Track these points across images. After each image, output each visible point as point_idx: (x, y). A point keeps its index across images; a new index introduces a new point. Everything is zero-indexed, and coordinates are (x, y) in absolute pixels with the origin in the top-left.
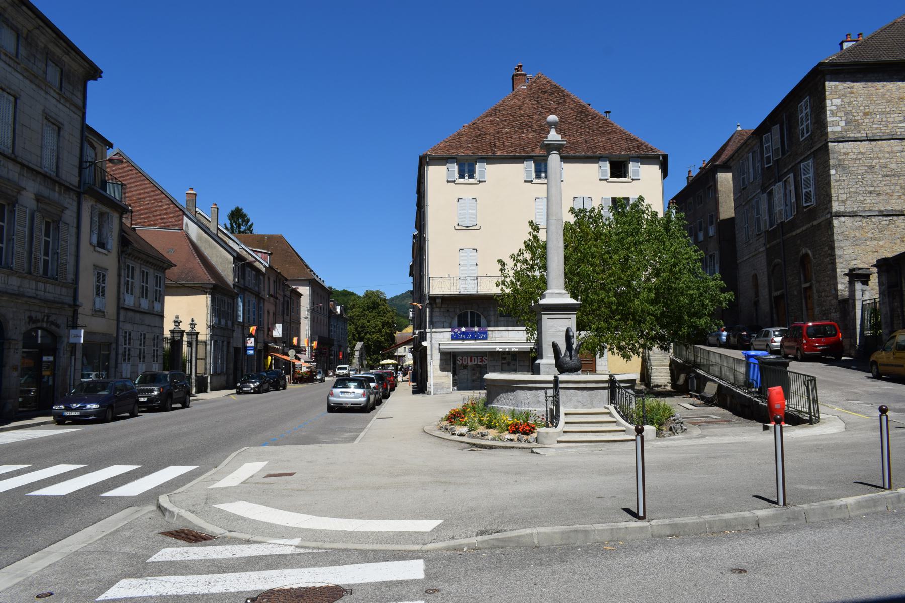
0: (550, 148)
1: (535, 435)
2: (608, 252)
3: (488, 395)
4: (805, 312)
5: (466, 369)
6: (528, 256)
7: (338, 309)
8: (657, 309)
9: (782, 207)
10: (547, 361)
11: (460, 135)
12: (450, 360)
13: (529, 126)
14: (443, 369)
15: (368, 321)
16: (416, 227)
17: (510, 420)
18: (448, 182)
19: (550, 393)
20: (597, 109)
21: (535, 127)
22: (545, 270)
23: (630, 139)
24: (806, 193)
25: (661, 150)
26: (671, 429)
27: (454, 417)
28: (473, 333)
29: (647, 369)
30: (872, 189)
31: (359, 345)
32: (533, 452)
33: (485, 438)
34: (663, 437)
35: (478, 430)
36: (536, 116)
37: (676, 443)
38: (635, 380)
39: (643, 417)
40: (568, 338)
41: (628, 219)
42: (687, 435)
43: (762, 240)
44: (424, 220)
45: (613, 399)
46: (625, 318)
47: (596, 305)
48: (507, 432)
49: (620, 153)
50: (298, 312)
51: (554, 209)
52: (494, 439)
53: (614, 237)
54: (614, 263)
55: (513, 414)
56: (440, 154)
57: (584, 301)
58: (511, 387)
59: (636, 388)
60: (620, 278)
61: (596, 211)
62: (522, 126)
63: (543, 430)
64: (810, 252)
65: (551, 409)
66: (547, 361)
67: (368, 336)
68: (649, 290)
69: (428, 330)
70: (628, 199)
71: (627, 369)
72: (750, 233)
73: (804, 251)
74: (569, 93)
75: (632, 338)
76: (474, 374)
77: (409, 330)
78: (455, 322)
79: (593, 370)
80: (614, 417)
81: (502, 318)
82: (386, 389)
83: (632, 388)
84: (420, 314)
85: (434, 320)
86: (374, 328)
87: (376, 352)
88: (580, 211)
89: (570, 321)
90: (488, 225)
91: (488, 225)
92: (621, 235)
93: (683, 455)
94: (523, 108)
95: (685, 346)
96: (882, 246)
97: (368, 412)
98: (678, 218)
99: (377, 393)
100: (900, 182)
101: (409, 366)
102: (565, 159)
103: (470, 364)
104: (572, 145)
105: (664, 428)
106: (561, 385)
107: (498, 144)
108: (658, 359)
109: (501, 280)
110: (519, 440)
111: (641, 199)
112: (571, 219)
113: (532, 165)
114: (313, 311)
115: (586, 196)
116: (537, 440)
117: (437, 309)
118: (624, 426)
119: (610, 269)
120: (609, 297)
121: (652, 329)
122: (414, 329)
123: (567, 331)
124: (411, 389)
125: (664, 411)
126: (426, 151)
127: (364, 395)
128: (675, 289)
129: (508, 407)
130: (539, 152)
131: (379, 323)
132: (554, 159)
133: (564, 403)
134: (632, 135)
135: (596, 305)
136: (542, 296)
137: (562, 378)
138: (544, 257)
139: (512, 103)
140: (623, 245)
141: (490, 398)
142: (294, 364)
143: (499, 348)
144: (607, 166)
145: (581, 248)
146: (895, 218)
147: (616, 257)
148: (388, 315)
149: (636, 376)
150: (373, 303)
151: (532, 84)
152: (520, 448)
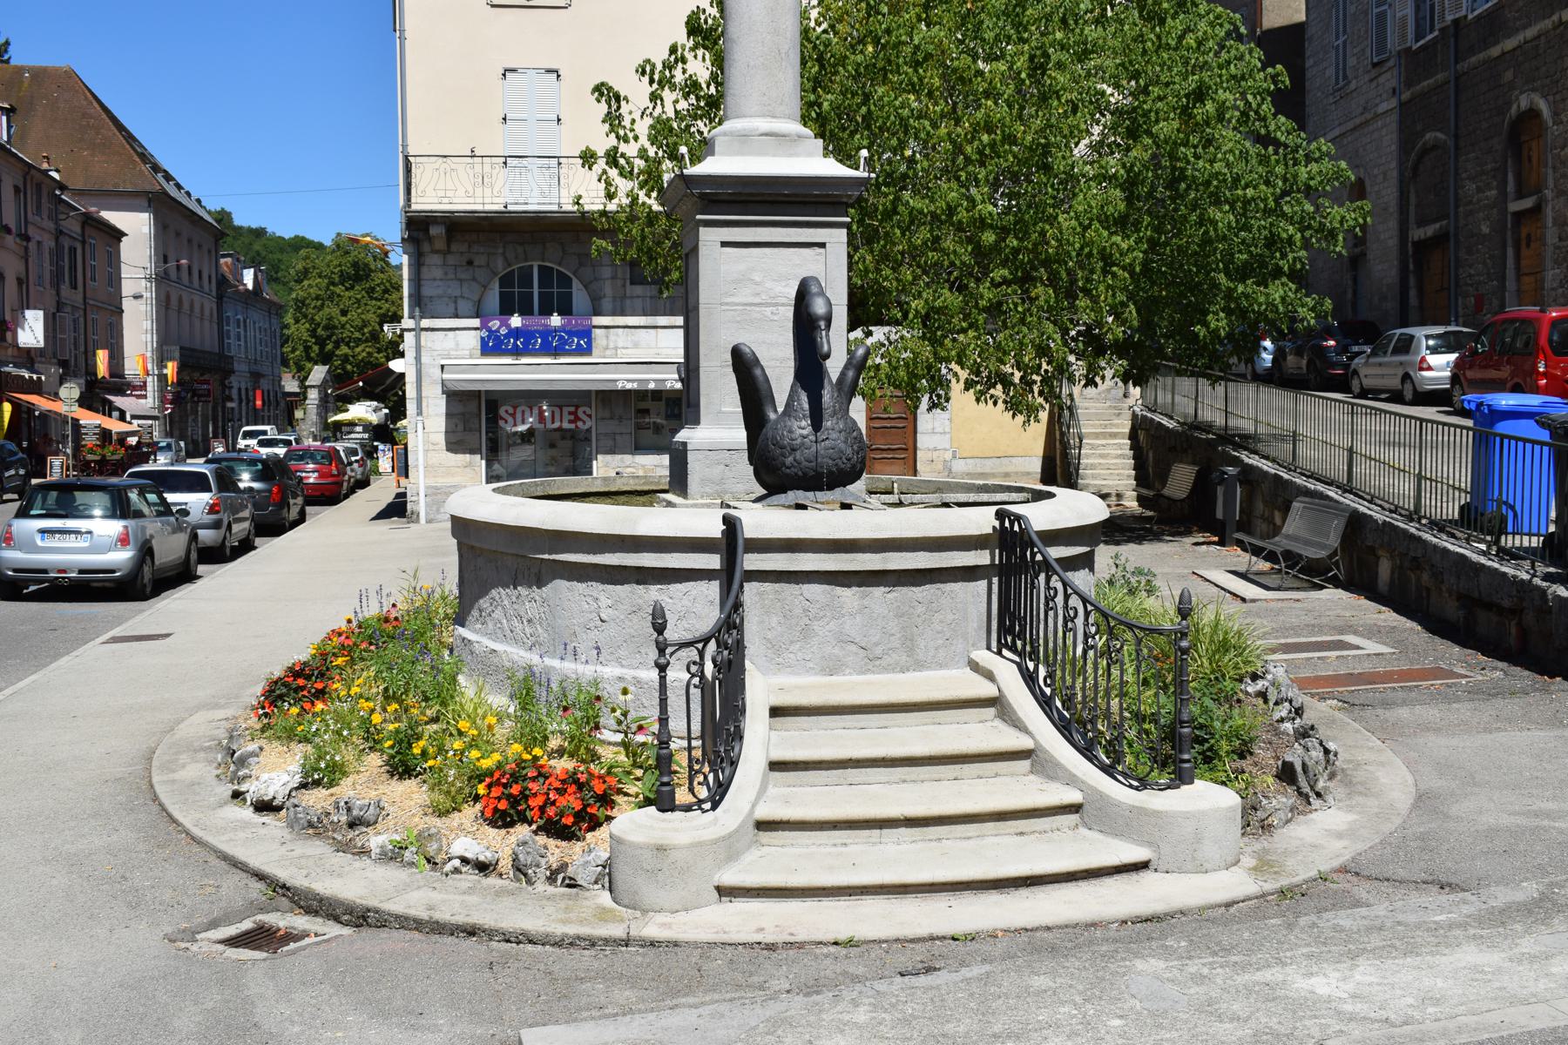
4: (1511, 284)
7: (248, 277)
10: (718, 431)
14: (454, 445)
15: (344, 313)
28: (548, 333)
29: (1065, 446)
31: (318, 373)
40: (807, 327)
43: (1389, 79)
45: (1011, 627)
50: (115, 280)
64: (1543, 106)
66: (718, 431)
67: (344, 350)
72: (1351, 61)
73: (1524, 102)
78: (493, 299)
81: (638, 290)
85: (427, 291)
86: (360, 329)
89: (826, 259)
106: (752, 562)
108: (1098, 416)
114: (162, 278)
116: (608, 876)
117: (435, 259)
118: (1072, 780)
127: (124, 541)
131: (372, 317)
133: (775, 648)
142: (75, 421)
143: (626, 380)
150: (355, 265)
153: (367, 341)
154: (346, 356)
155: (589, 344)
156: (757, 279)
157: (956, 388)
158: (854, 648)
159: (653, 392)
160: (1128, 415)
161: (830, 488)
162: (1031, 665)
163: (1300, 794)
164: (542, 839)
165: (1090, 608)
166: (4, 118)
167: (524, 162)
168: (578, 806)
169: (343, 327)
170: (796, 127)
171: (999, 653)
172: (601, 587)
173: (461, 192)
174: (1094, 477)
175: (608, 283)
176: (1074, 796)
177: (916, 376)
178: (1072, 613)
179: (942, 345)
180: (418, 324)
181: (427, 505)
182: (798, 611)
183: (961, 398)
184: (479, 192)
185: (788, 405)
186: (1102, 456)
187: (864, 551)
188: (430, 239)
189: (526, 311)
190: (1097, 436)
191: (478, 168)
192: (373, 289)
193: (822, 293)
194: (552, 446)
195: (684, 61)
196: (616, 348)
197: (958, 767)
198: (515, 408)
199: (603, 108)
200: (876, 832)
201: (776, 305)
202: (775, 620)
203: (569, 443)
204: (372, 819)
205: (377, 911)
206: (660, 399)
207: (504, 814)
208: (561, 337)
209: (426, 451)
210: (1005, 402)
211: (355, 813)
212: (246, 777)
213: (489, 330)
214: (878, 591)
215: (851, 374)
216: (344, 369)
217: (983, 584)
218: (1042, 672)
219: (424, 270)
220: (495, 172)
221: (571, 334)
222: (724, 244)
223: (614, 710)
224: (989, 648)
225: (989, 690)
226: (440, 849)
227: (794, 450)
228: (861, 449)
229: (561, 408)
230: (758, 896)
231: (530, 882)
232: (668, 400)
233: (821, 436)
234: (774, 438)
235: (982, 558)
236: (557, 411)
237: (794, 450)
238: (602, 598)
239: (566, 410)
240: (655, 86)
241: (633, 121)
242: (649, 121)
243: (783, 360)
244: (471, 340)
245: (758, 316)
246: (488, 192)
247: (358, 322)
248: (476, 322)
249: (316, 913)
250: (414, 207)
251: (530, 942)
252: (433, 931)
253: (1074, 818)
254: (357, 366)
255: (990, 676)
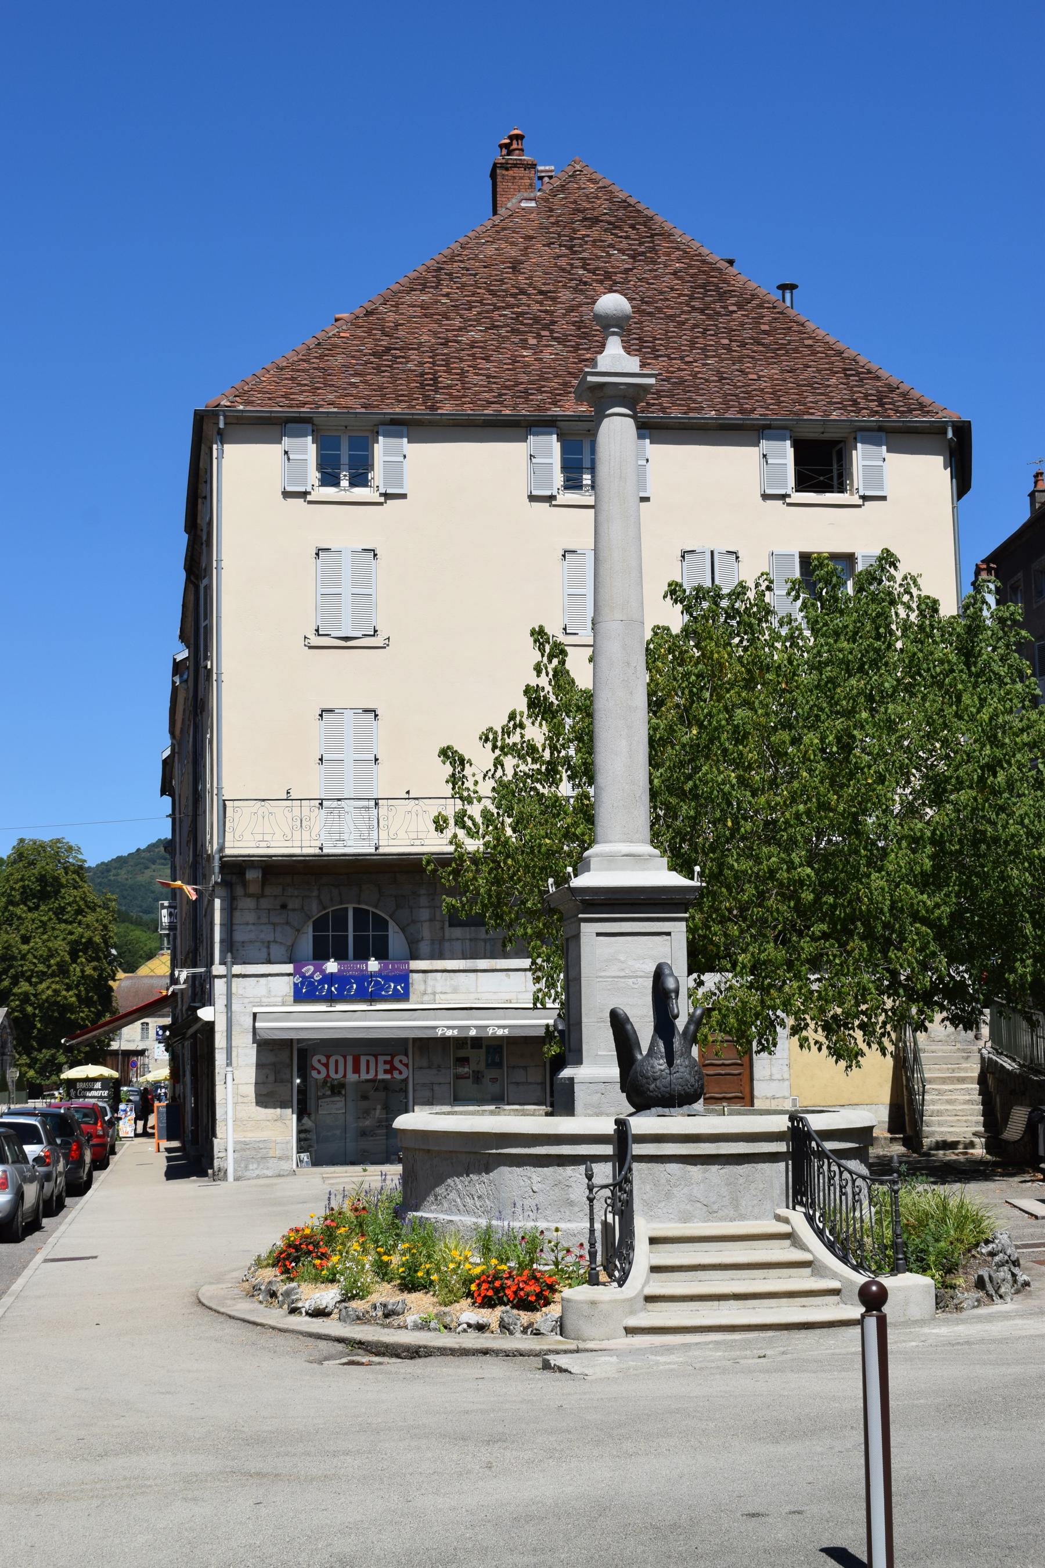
0: (605, 397)
1: (554, 1311)
2: (786, 725)
3: (407, 1178)
5: (338, 1096)
6: (536, 733)
8: (938, 903)
10: (596, 1069)
11: (325, 348)
12: (290, 1068)
13: (544, 325)
14: (265, 1098)
15: (25, 940)
16: (182, 637)
17: (475, 1264)
18: (287, 495)
19: (604, 1173)
20: (755, 276)
21: (563, 327)
22: (591, 782)
23: (855, 372)
25: (951, 409)
26: (980, 1284)
27: (297, 1255)
28: (364, 978)
29: (911, 1092)
32: (547, 1366)
33: (395, 1321)
34: (958, 1308)
35: (375, 1298)
36: (565, 295)
37: (996, 1329)
38: (870, 1129)
39: (894, 1245)
40: (662, 997)
41: (847, 620)
42: (1032, 1303)
44: (208, 614)
45: (800, 1190)
46: (840, 932)
47: (750, 890)
48: (466, 1302)
49: (826, 412)
51: (616, 587)
52: (424, 1326)
53: (805, 678)
54: (805, 759)
55: (486, 1243)
56: (260, 406)
57: (713, 877)
58: (479, 1155)
59: (874, 1151)
60: (824, 806)
61: (751, 594)
62: (521, 326)
63: (581, 1293)
65: (605, 1224)
66: (596, 1069)
67: (24, 987)
68: (916, 842)
69: (218, 969)
70: (850, 558)
71: (852, 1096)
74: (668, 226)
75: (863, 993)
76: (367, 1112)
77: (159, 966)
78: (306, 944)
79: (743, 1096)
80: (803, 1247)
81: (458, 932)
82: (80, 1162)
83: (859, 1154)
84: (195, 918)
85: (239, 936)
86: (44, 960)
87: (48, 1041)
88: (700, 593)
89: (668, 944)
90: (412, 632)
91: (412, 632)
92: (828, 672)
93: (1016, 1370)
94: (526, 267)
95: (1029, 1019)
97: (16, 1238)
98: (1002, 621)
99: (48, 1177)
101: (157, 1085)
102: (653, 429)
103: (352, 1077)
104: (677, 386)
105: (960, 1281)
106: (637, 1149)
107: (445, 380)
109: (451, 808)
110: (504, 1326)
111: (888, 559)
112: (675, 619)
113: (552, 446)
115: (721, 547)
116: (561, 1327)
117: (249, 903)
118: (835, 1276)
119: (793, 776)
120: (791, 866)
121: (925, 966)
122: (174, 966)
123: (659, 975)
124: (163, 1164)
125: (960, 1227)
126: (216, 394)
128: (996, 840)
129: (469, 1220)
130: (571, 407)
131: (61, 945)
132: (617, 431)
134: (862, 360)
135: (750, 890)
136: (581, 865)
137: (642, 1124)
138: (586, 739)
139: (490, 250)
140: (832, 702)
141: (415, 1191)
143: (446, 1027)
144: (784, 454)
145: (701, 710)
147: (811, 738)
148: (90, 918)
149: (874, 1114)
150: (42, 879)
151: (554, 193)
152: (507, 1354)
153: (53, 975)
154: (26, 994)
155: (406, 989)
157: (782, 1033)
158: (699, 1205)
159: (473, 1039)
160: (977, 1058)
161: (680, 1106)
162: (811, 1212)
163: (988, 1295)
164: (515, 1311)
165: (855, 1177)
166: (1041, 1153)
167: (343, 803)
168: (538, 1290)
169: (24, 957)
170: (649, 849)
171: (794, 1209)
172: (533, 1169)
173: (279, 836)
174: (940, 1124)
175: (426, 925)
176: (835, 1284)
177: (745, 1023)
178: (844, 1183)
179: (768, 993)
180: (229, 970)
181: (235, 1161)
182: (663, 1181)
183: (785, 1042)
184: (297, 835)
185: (651, 1049)
186: (949, 1102)
187: (704, 1142)
188: (244, 884)
189: (340, 957)
190: (944, 1081)
191: (296, 811)
192: (62, 910)
193: (672, 974)
194: (365, 1098)
195: (522, 726)
196: (434, 994)
197: (766, 1271)
198: (328, 1057)
199: (448, 769)
200: (716, 1303)
201: (637, 977)
202: (648, 1188)
203: (382, 1095)
204: (401, 1311)
205: (425, 1347)
206: (480, 1047)
207: (490, 1298)
208: (377, 983)
209: (235, 1104)
210: (829, 1047)
211: (390, 1307)
212: (297, 1300)
213: (303, 976)
214: (714, 1168)
215: (692, 1027)
216: (23, 1011)
217: (783, 1165)
218: (818, 1214)
219: (237, 914)
220: (313, 815)
221: (387, 979)
222: (598, 934)
223: (550, 1242)
224: (788, 1207)
225: (785, 1228)
226: (452, 1321)
227: (655, 1080)
228: (701, 1079)
229: (376, 1057)
230: (649, 1333)
231: (511, 1333)
232: (488, 1047)
233: (673, 1070)
234: (641, 1071)
235: (781, 1147)
236: (372, 1060)
237: (655, 1080)
238: (534, 1177)
239: (381, 1059)
240: (498, 752)
241: (476, 783)
242: (491, 783)
243: (883, 1122)
244: (284, 987)
246: (306, 835)
247: (43, 952)
248: (289, 968)
249: (383, 1355)
250: (228, 852)
251: (521, 1355)
252: (462, 1355)
253: (836, 1298)
254: (40, 1007)
255: (786, 1221)
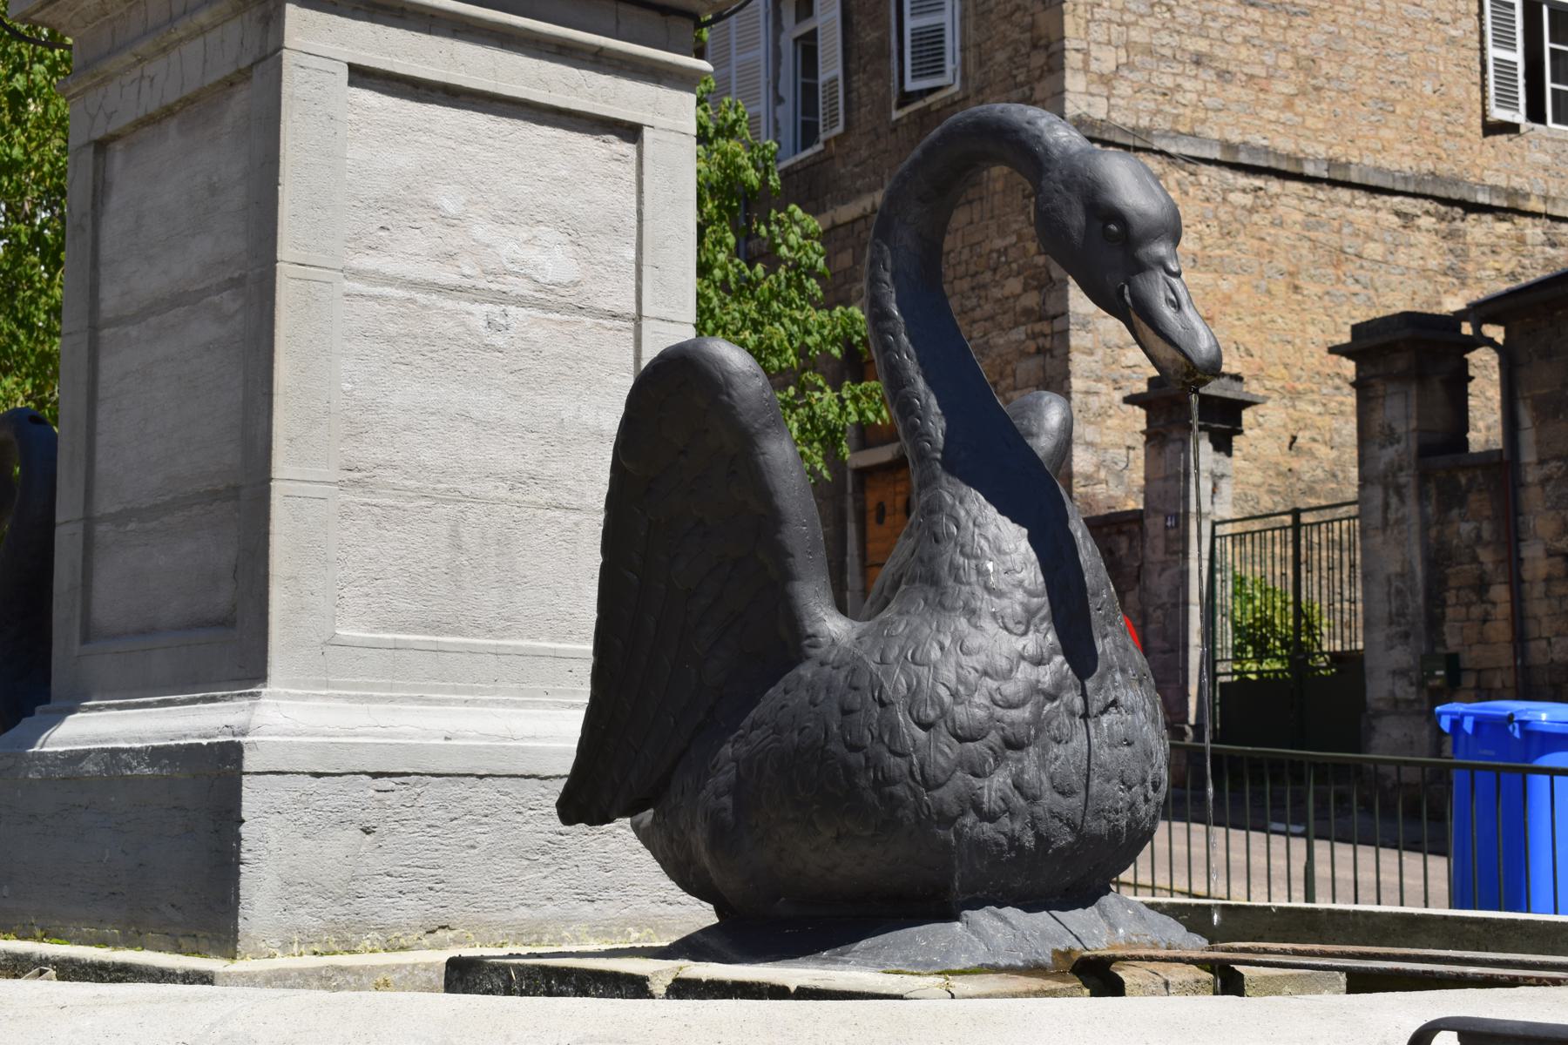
9: (761, 108)
24: (917, 34)
30: (1202, 45)
96: (1227, 300)
100: (1292, 36)
146: (1274, 186)
156: (451, 208)
201: (502, 298)
222: (361, 76)
245: (450, 327)
